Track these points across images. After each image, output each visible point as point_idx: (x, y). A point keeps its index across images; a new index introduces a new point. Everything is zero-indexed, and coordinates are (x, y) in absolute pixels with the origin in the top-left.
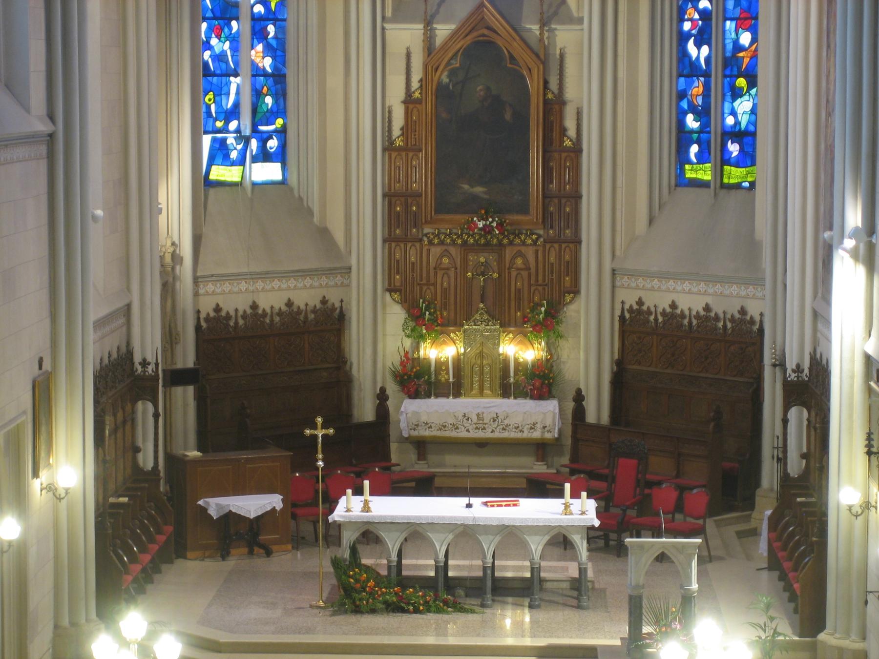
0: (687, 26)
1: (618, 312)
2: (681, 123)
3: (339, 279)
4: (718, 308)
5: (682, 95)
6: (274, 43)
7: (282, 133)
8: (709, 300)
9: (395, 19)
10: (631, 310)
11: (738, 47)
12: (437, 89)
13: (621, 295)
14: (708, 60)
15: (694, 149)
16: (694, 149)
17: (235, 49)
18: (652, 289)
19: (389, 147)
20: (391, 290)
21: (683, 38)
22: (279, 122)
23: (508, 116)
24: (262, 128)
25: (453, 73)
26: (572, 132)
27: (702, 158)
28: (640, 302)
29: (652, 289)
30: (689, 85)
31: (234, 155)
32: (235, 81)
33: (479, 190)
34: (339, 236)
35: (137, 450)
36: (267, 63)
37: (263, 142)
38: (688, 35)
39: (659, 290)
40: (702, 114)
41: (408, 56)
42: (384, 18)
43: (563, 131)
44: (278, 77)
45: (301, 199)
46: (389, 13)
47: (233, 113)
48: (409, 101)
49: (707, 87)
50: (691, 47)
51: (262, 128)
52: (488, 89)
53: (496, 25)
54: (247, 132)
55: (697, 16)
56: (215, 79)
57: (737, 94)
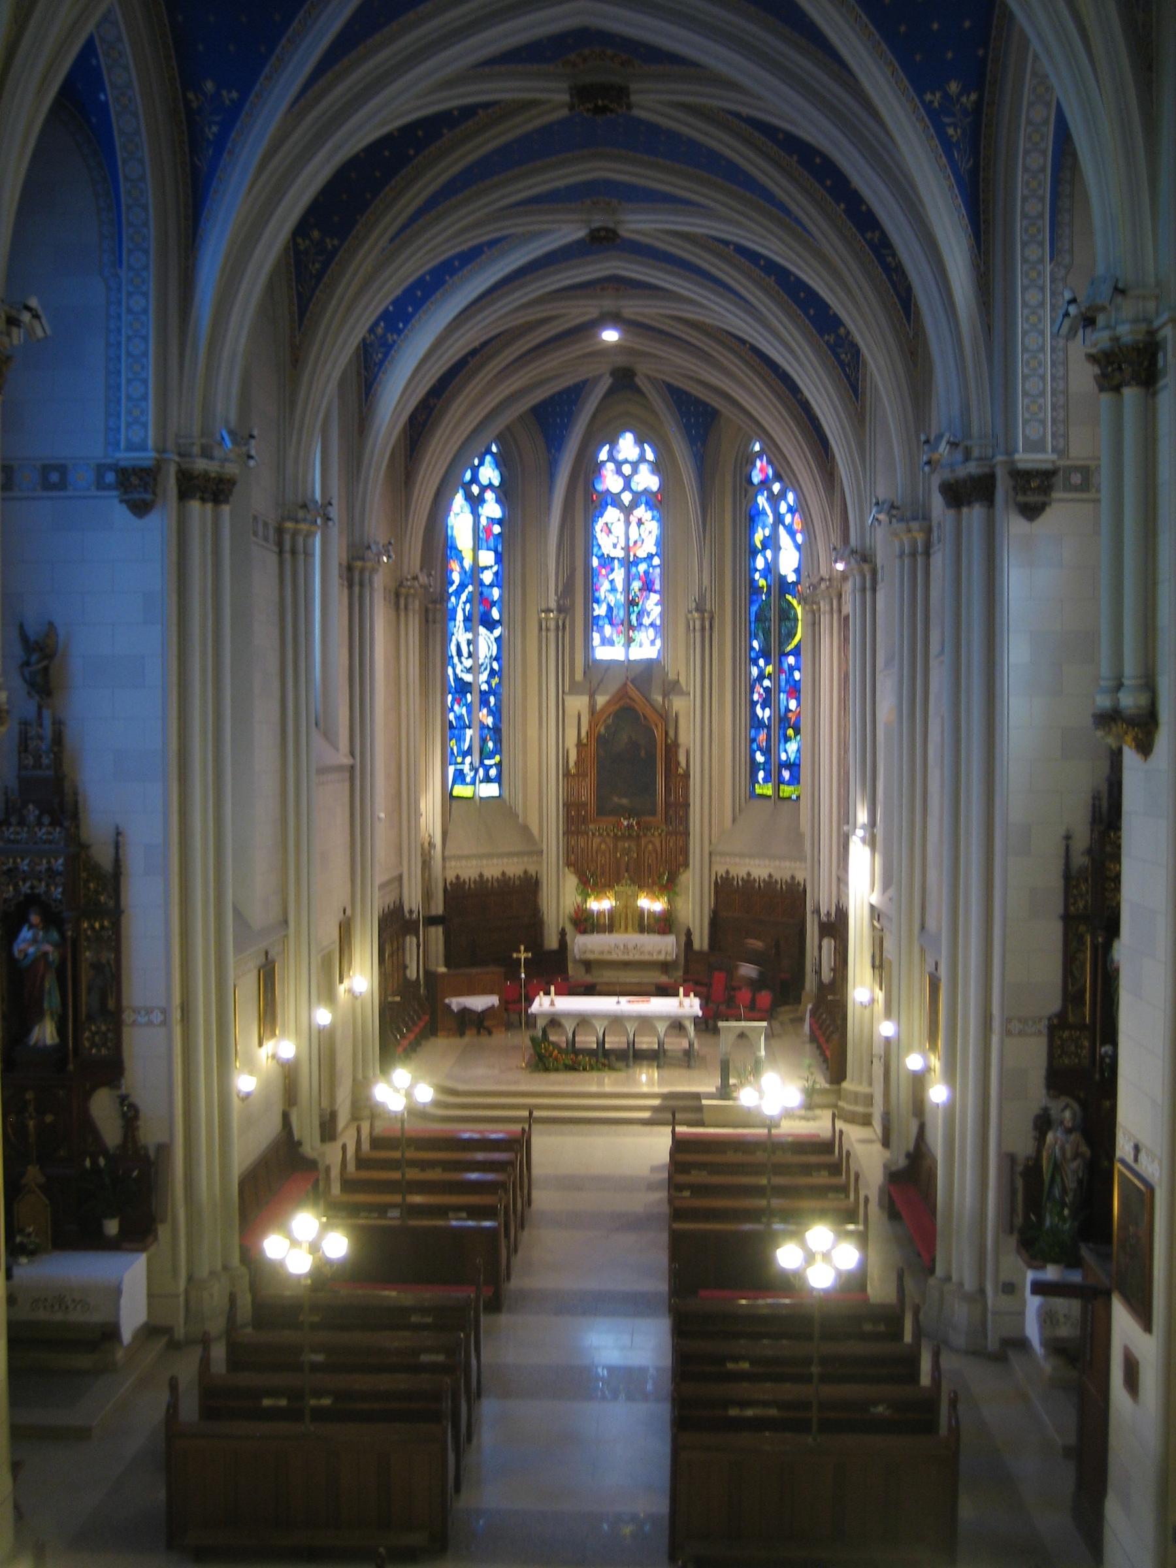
0: (756, 697)
2: (753, 759)
4: (777, 876)
7: (499, 765)
11: (788, 710)
12: (597, 740)
13: (715, 868)
14: (769, 718)
15: (761, 774)
16: (761, 774)
17: (469, 712)
19: (567, 774)
21: (753, 704)
22: (497, 758)
23: (643, 754)
25: (607, 728)
30: (758, 734)
31: (468, 779)
32: (469, 732)
34: (535, 830)
36: (489, 721)
40: (766, 752)
44: (496, 730)
45: (511, 807)
46: (567, 689)
48: (579, 744)
55: (762, 691)
57: (787, 739)
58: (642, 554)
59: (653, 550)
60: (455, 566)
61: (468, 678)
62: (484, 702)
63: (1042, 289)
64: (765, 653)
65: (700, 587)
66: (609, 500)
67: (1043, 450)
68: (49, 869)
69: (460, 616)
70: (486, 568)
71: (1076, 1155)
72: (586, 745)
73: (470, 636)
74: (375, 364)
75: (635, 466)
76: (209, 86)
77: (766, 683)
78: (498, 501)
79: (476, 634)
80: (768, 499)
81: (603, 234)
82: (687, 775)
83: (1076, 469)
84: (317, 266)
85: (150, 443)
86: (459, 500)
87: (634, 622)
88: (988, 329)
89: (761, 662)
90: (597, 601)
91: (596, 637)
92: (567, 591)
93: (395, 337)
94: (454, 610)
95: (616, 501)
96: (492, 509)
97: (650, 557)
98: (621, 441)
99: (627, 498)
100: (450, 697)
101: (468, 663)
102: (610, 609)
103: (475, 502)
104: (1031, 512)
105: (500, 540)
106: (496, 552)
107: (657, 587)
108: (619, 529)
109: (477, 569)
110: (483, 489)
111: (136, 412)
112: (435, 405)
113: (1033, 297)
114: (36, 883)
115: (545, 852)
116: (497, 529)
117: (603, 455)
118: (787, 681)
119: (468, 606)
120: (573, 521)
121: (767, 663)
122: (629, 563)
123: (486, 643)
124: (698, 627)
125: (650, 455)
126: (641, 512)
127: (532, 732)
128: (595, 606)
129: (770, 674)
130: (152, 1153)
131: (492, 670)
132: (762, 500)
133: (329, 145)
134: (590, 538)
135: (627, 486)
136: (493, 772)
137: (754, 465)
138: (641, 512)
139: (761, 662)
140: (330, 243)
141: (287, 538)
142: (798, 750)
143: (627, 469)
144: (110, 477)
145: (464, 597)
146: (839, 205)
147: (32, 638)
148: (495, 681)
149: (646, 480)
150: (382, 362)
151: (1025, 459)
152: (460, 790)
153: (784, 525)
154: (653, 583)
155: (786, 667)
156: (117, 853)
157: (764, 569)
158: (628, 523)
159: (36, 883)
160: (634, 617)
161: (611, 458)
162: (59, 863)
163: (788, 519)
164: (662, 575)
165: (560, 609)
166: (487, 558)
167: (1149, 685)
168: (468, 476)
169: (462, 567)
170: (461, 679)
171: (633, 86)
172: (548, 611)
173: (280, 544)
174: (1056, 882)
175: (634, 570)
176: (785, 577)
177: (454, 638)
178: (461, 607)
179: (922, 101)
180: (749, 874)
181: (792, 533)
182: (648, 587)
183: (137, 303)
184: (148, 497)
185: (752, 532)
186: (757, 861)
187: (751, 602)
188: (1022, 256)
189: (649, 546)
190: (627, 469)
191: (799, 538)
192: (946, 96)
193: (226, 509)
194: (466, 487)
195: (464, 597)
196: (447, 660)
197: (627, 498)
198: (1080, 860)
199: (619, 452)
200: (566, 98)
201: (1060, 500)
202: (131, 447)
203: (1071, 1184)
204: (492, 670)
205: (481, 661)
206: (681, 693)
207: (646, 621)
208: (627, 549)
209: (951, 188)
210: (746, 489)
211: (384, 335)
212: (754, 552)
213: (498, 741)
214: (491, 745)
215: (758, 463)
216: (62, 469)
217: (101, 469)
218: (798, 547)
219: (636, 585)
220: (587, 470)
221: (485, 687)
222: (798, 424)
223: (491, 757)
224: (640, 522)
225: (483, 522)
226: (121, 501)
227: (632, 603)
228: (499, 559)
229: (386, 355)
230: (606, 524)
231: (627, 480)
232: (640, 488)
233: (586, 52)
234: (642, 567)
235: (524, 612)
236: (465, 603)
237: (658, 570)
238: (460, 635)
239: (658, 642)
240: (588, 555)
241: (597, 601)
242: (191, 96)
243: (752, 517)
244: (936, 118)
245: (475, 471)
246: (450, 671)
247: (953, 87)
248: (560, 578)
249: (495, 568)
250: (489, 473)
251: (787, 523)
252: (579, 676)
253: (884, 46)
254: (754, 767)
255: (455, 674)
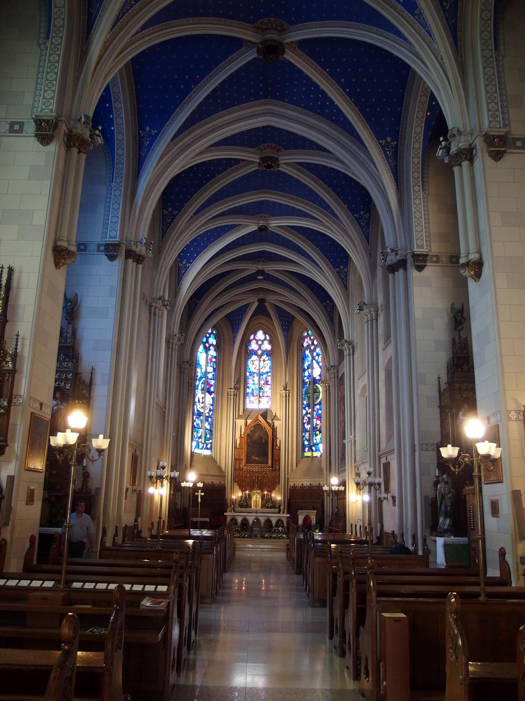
0: (305, 421)
1: (289, 488)
2: (303, 443)
3: (175, 689)
4: (313, 484)
5: (304, 437)
6: (210, 423)
7: (211, 443)
8: (311, 482)
9: (238, 419)
10: (292, 486)
11: (317, 425)
13: (290, 484)
15: (307, 449)
16: (307, 449)
17: (201, 423)
18: (297, 481)
19: (236, 447)
20: (235, 481)
21: (304, 424)
22: (210, 441)
23: (264, 441)
24: (206, 442)
25: (251, 431)
26: (278, 445)
27: (309, 451)
28: (294, 485)
29: (297, 481)
30: (305, 434)
32: (201, 430)
33: (257, 458)
34: (224, 469)
35: (176, 504)
36: (208, 427)
37: (207, 445)
38: (305, 423)
39: (299, 481)
40: (309, 440)
41: (241, 427)
42: (235, 418)
43: (277, 445)
44: (211, 431)
45: (215, 459)
47: (200, 437)
48: (241, 437)
49: (310, 434)
50: (306, 426)
51: (206, 442)
52: (259, 435)
53: (261, 420)
54: (203, 442)
55: (307, 418)
56: (196, 429)
57: (316, 435)
58: (264, 371)
59: (269, 370)
60: (198, 370)
61: (202, 410)
62: (207, 420)
63: (420, 199)
64: (308, 405)
65: (285, 383)
66: (253, 353)
67: (423, 248)
68: (66, 378)
69: (200, 388)
70: (209, 373)
71: (449, 493)
72: (243, 437)
73: (203, 395)
74: (182, 274)
75: (263, 341)
76: (148, 129)
77: (309, 416)
78: (215, 350)
79: (205, 396)
80: (310, 352)
81: (263, 227)
82: (280, 449)
83: (435, 256)
84: (170, 220)
85: (118, 236)
86: (201, 348)
87: (261, 395)
88: (402, 215)
89: (307, 408)
90: (248, 388)
91: (247, 400)
92: (238, 382)
93: (189, 265)
94: (198, 386)
95: (255, 353)
96: (212, 352)
97: (267, 373)
98: (258, 333)
99: (259, 352)
100: (195, 417)
101: (202, 405)
102: (253, 390)
103: (207, 349)
104: (420, 268)
105: (215, 364)
106: (213, 367)
107: (270, 383)
108: (257, 363)
109: (206, 373)
110: (210, 345)
111: (114, 227)
112: (198, 303)
113: (417, 202)
114: (60, 383)
115: (227, 476)
116: (214, 360)
117: (252, 337)
118: (316, 414)
119: (203, 385)
120: (241, 359)
121: (309, 409)
122: (260, 374)
123: (209, 399)
124: (284, 396)
125: (268, 338)
126: (264, 357)
127: (224, 432)
128: (247, 389)
129: (310, 412)
130: (93, 491)
131: (210, 409)
132: (307, 352)
133: (184, 155)
134: (246, 365)
135: (260, 348)
136: (209, 446)
137: (304, 340)
138: (264, 357)
139: (307, 408)
140: (175, 212)
141: (153, 309)
142: (321, 439)
143: (260, 343)
144: (102, 248)
145: (201, 382)
146: (345, 205)
147: (68, 297)
148: (211, 413)
149: (267, 346)
150: (184, 273)
151: (417, 250)
152: (197, 451)
153: (315, 360)
154: (268, 381)
155: (316, 409)
156: (91, 376)
157: (308, 376)
158: (260, 361)
159: (60, 383)
160: (261, 394)
161: (254, 339)
162: (70, 376)
163: (317, 358)
164: (272, 380)
165: (235, 388)
166: (210, 369)
167: (479, 252)
168: (205, 340)
169: (201, 371)
170: (199, 410)
171: (280, 158)
172: (231, 389)
173: (150, 311)
174: (435, 394)
175: (261, 377)
176: (315, 378)
177: (197, 396)
178: (200, 384)
179: (379, 143)
180: (302, 485)
181: (318, 363)
182: (266, 383)
183: (117, 193)
184: (115, 254)
185: (303, 363)
186: (305, 480)
187: (303, 388)
188: (413, 189)
189: (267, 369)
190: (260, 343)
191: (321, 364)
192: (386, 142)
193: (141, 266)
194: (204, 344)
195: (201, 382)
196: (194, 403)
197: (259, 352)
198: (444, 387)
199: (257, 336)
200: (258, 161)
201: (428, 266)
202: (111, 237)
203: (449, 504)
204: (210, 409)
205: (206, 405)
206: (278, 420)
207: (265, 395)
208: (259, 369)
209: (389, 170)
210: (301, 349)
211: (185, 264)
212: (304, 370)
213: (211, 435)
214: (208, 436)
215: (306, 340)
216: (85, 245)
217: (99, 246)
218: (320, 367)
219: (262, 382)
220: (246, 342)
221: (207, 415)
222: (322, 311)
223: (208, 441)
224: (264, 361)
225: (209, 357)
226: (106, 255)
227: (260, 388)
228: (214, 370)
229: (186, 271)
230: (252, 361)
231: (260, 346)
232: (264, 349)
233: (266, 145)
234: (265, 376)
235: (222, 390)
236: (202, 384)
237: (270, 377)
238: (199, 395)
239: (270, 403)
240: (245, 372)
241: (248, 388)
242: (141, 132)
243: (303, 358)
244: (384, 148)
245: (207, 339)
246: (195, 407)
247: (389, 139)
248: (236, 378)
249: (213, 373)
250: (212, 341)
251: (316, 359)
252: (241, 413)
253: (367, 124)
254: (304, 446)
255: (197, 409)
